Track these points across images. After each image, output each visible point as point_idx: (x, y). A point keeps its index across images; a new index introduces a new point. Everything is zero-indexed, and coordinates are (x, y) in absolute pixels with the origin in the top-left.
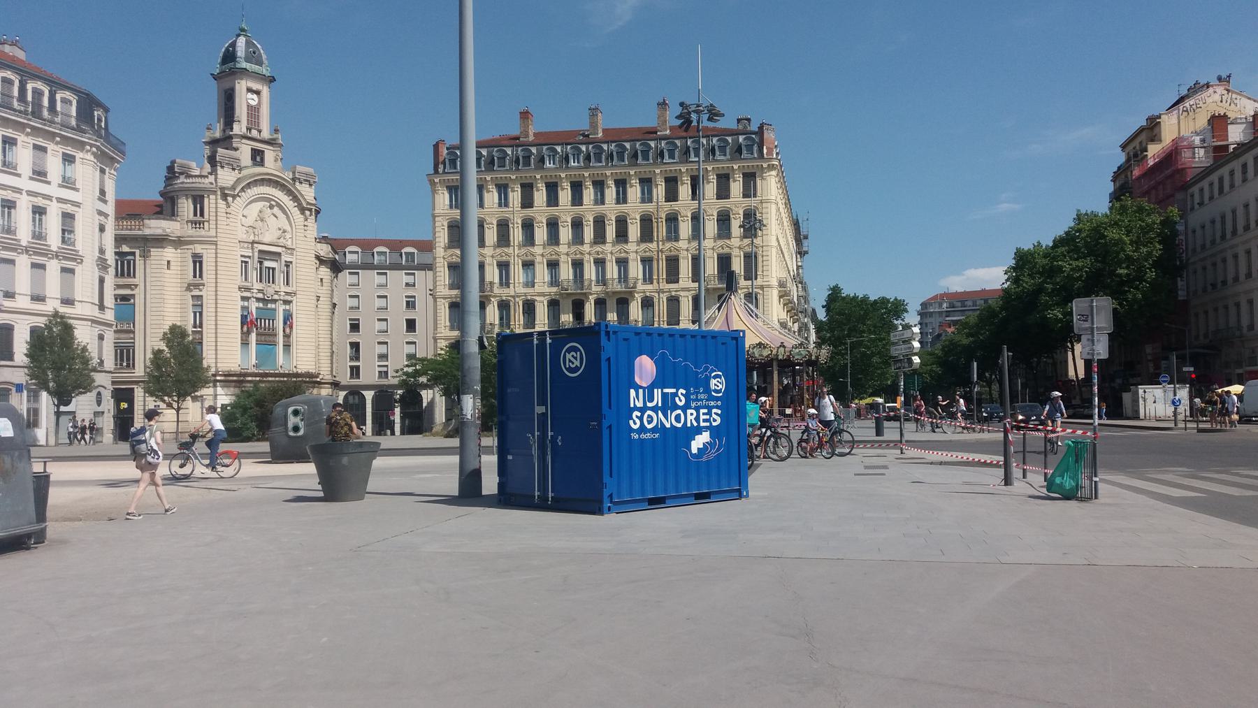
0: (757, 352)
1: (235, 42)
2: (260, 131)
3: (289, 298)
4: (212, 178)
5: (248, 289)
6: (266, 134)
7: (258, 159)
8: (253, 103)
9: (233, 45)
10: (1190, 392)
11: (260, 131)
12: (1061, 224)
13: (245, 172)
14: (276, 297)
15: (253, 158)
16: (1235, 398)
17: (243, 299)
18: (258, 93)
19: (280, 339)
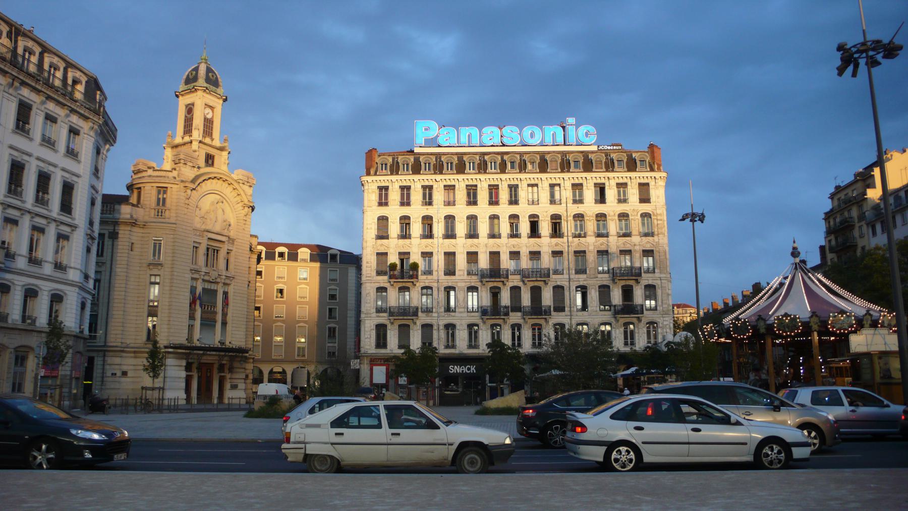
0: (197, 219)
1: (198, 67)
2: (212, 140)
3: (228, 281)
4: (175, 173)
5: (197, 271)
6: (217, 143)
7: (210, 162)
8: (209, 116)
9: (196, 69)
10: (396, 357)
11: (212, 140)
12: (822, 227)
13: (202, 171)
14: (218, 280)
15: (207, 161)
16: (437, 359)
17: (193, 279)
18: (212, 108)
19: (219, 318)
